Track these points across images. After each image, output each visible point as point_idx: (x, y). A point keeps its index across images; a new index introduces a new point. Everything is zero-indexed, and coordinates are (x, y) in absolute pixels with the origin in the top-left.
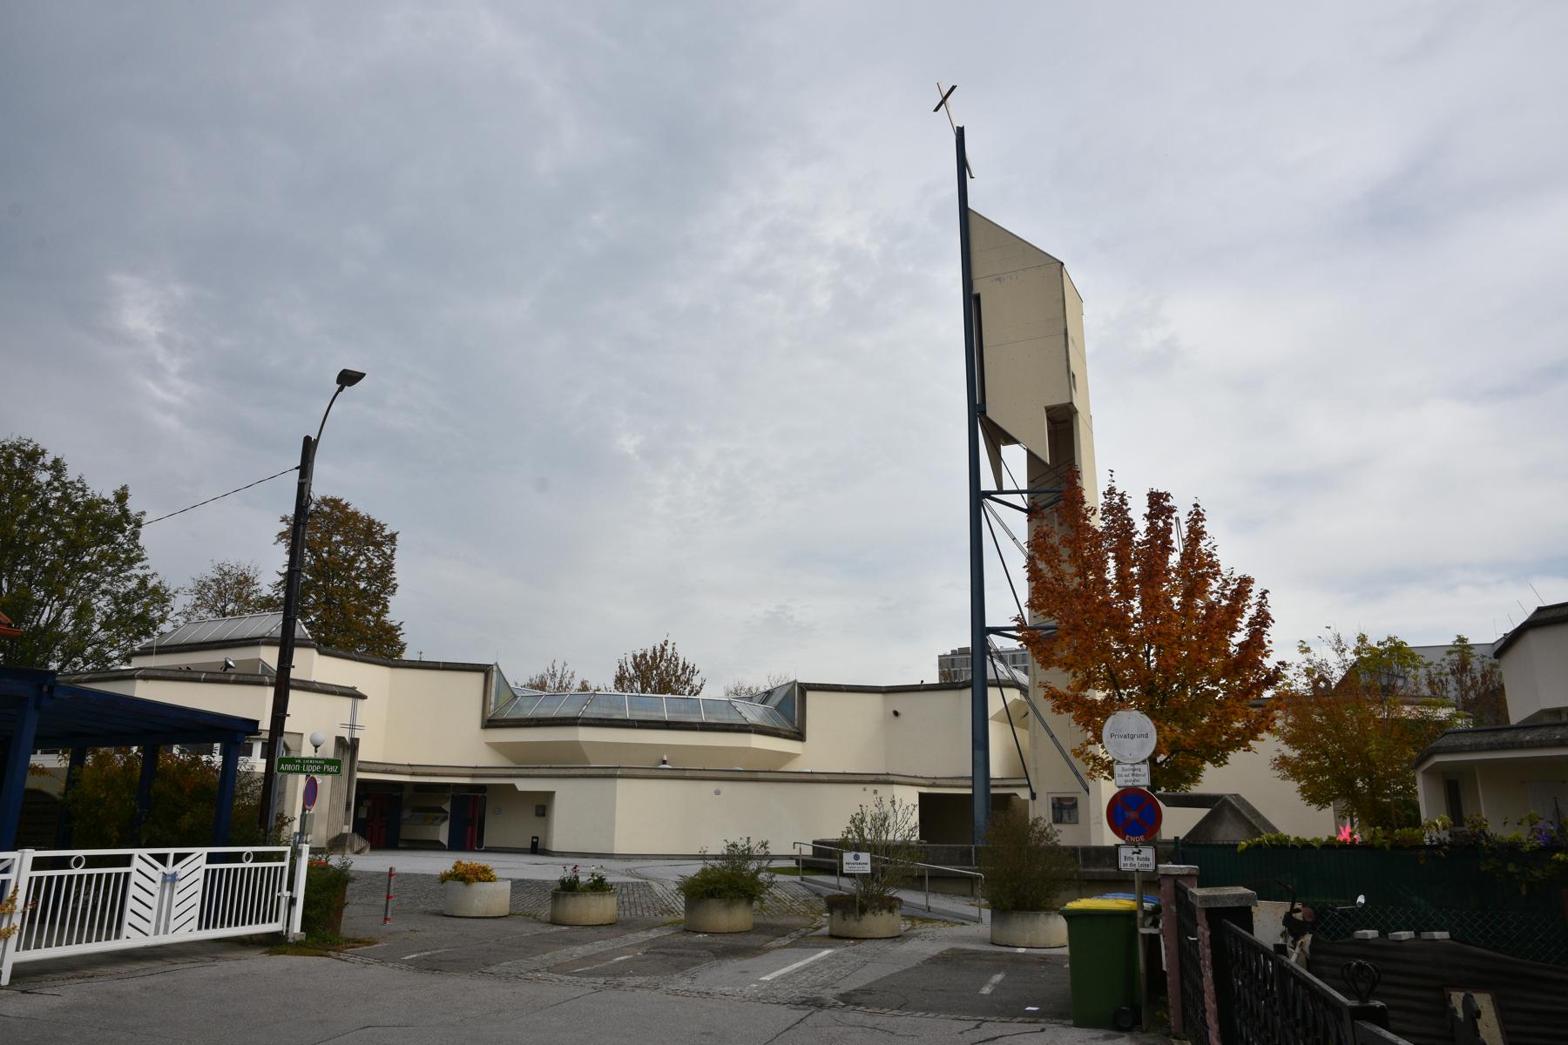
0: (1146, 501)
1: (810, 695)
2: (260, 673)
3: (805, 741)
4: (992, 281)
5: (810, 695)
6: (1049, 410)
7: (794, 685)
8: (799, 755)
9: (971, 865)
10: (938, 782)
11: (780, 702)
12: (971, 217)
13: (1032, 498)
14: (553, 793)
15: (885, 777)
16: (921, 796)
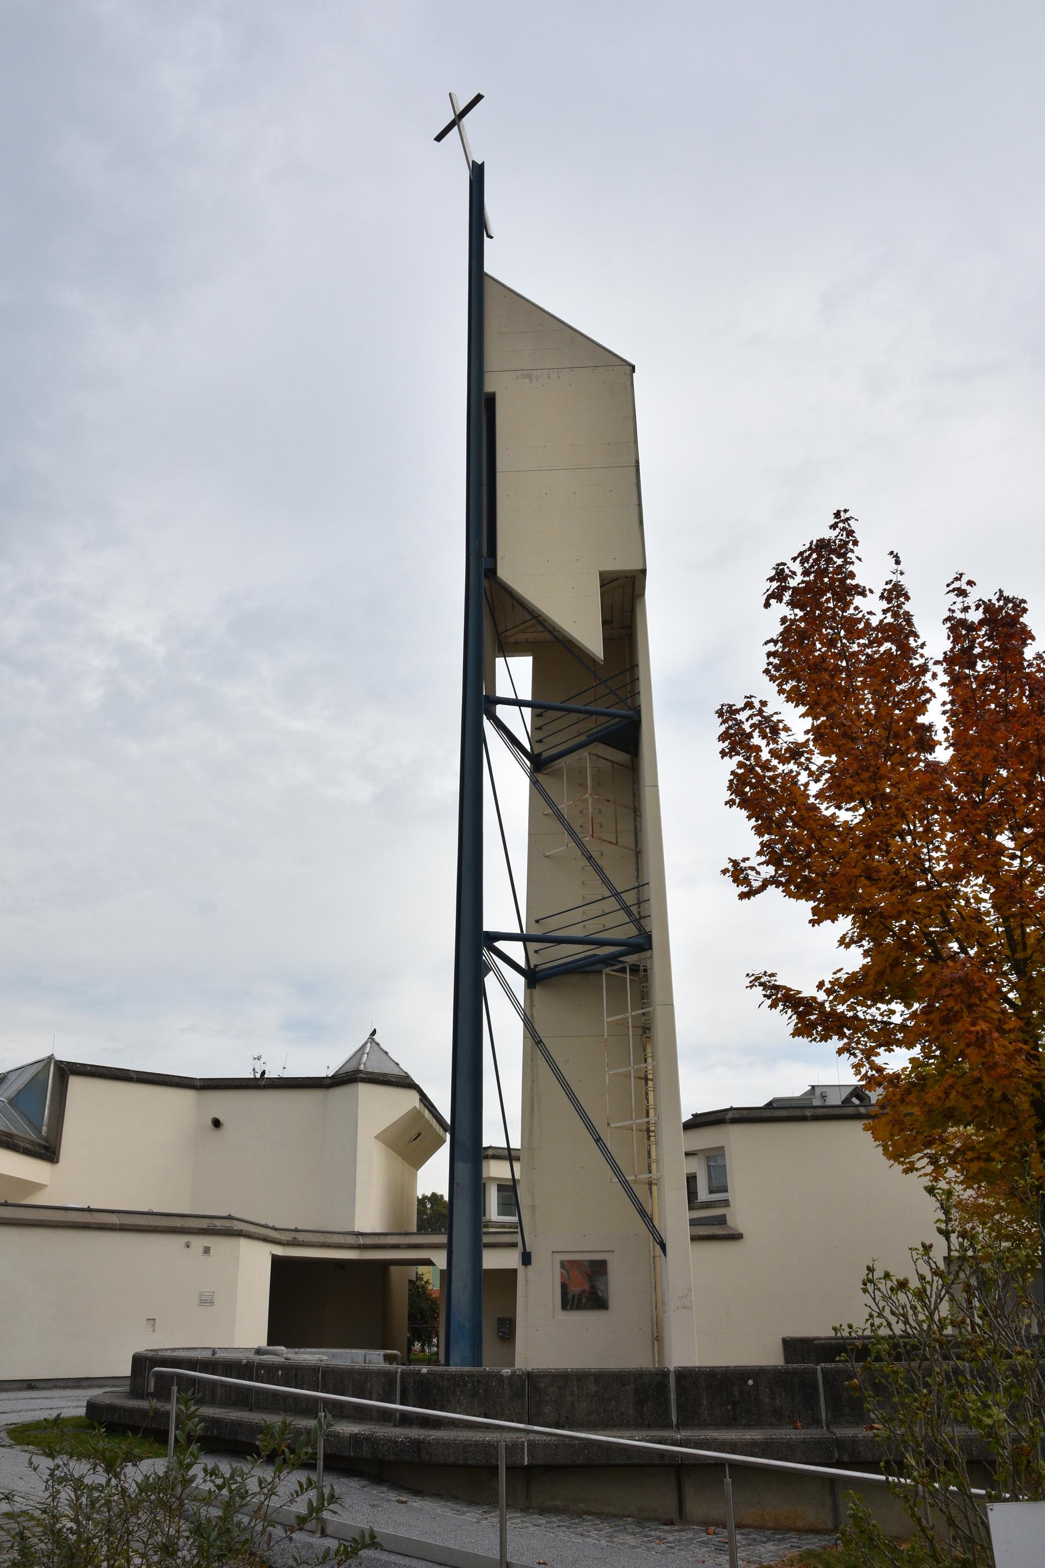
0: (944, 630)
1: (75, 1084)
2: (152, 1389)
3: (58, 1162)
4: (518, 378)
5: (75, 1084)
6: (602, 575)
7: (49, 1063)
8: (45, 1186)
9: (667, 1425)
10: (301, 1237)
11: (20, 1092)
12: (488, 287)
13: (540, 728)
14: (725, 1215)
15: (227, 1224)
16: (277, 1263)
